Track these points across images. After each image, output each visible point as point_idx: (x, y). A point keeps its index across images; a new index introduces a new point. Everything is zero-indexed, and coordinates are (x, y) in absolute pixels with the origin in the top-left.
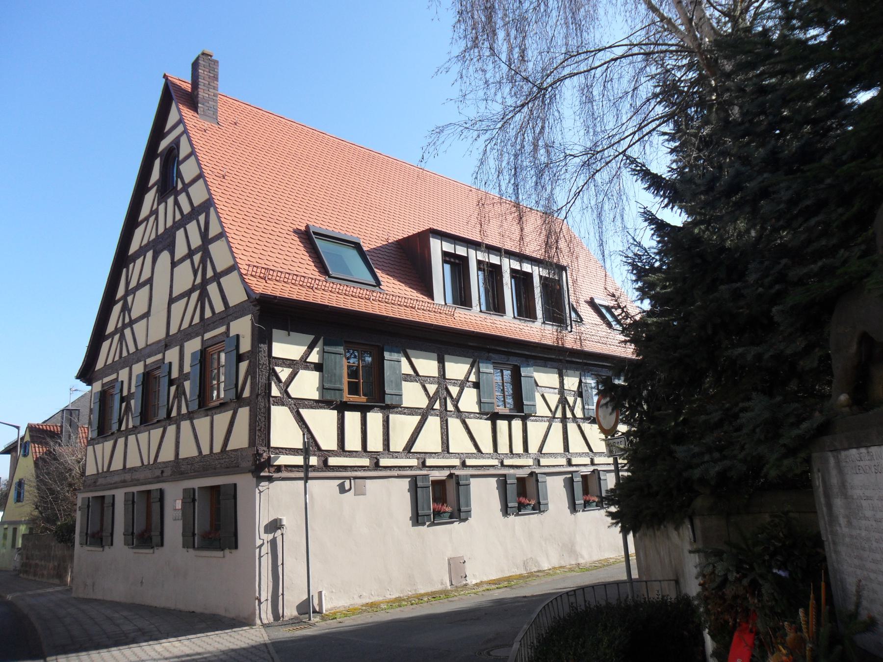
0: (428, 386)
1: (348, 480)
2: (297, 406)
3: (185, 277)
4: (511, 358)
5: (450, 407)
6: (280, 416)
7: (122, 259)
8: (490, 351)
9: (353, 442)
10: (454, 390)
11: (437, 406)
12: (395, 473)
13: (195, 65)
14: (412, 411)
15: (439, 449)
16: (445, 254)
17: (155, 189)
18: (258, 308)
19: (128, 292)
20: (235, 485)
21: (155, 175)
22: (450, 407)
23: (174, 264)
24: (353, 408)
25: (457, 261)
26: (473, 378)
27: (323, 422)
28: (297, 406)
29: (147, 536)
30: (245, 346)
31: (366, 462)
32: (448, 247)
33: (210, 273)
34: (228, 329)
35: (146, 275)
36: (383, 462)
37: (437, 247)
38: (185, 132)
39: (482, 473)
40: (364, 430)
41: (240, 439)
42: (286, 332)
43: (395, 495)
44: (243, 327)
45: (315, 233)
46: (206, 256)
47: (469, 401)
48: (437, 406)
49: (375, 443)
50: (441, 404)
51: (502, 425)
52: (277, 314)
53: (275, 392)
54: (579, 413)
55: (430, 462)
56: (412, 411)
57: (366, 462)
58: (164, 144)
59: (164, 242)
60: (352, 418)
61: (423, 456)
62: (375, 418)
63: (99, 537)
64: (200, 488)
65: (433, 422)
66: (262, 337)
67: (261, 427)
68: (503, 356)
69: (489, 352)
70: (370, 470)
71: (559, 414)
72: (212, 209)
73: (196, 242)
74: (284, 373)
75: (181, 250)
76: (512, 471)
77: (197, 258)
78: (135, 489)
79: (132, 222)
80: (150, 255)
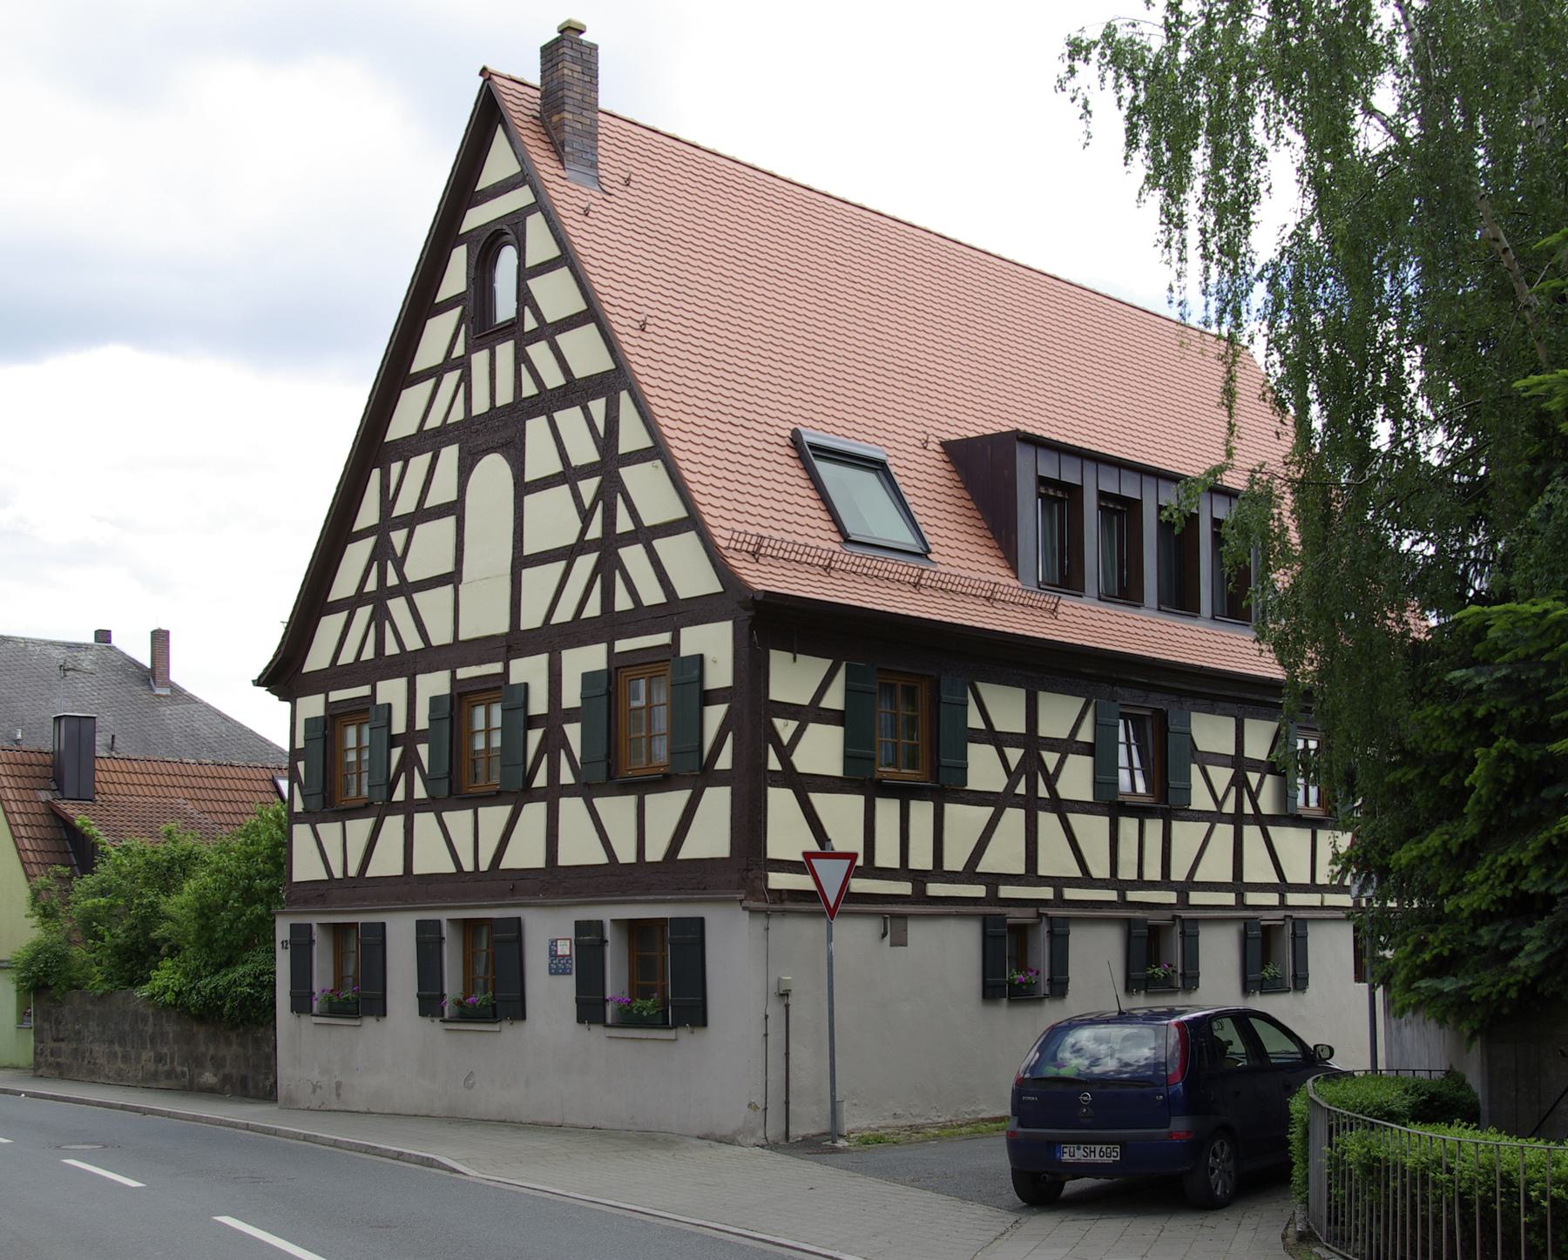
0: (1009, 751)
1: (893, 916)
2: (804, 786)
3: (554, 522)
4: (1152, 695)
5: (1043, 792)
6: (781, 802)
7: (372, 449)
8: (1115, 682)
9: (887, 856)
10: (1050, 759)
11: (1021, 789)
12: (953, 909)
13: (550, 54)
14: (980, 798)
15: (1021, 870)
16: (1042, 481)
17: (455, 314)
18: (752, 613)
19: (388, 522)
20: (702, 919)
21: (455, 280)
22: (1043, 792)
23: (523, 488)
24: (889, 791)
25: (1060, 494)
26: (1085, 735)
27: (842, 815)
28: (804, 786)
29: (497, 998)
30: (720, 675)
31: (905, 888)
32: (1048, 469)
33: (624, 524)
34: (676, 639)
35: (443, 490)
36: (934, 889)
37: (1027, 469)
38: (541, 205)
39: (1093, 913)
40: (904, 833)
41: (711, 836)
42: (790, 655)
43: (952, 950)
44: (713, 645)
45: (813, 447)
46: (612, 489)
47: (1076, 779)
48: (1021, 789)
49: (921, 859)
50: (1031, 793)
51: (1129, 826)
52: (773, 623)
53: (774, 764)
54: (1267, 804)
55: (1006, 892)
56: (980, 798)
57: (905, 888)
58: (476, 218)
59: (495, 433)
60: (887, 810)
61: (994, 880)
62: (922, 813)
63: (361, 999)
64: (613, 921)
65: (1014, 819)
66: (751, 668)
67: (749, 823)
68: (1138, 692)
69: (1113, 685)
70: (913, 903)
71: (1229, 808)
72: (624, 396)
73: (584, 452)
74: (785, 728)
75: (540, 459)
76: (1138, 914)
77: (588, 488)
78: (607, 914)
79: (396, 374)
80: (450, 455)
